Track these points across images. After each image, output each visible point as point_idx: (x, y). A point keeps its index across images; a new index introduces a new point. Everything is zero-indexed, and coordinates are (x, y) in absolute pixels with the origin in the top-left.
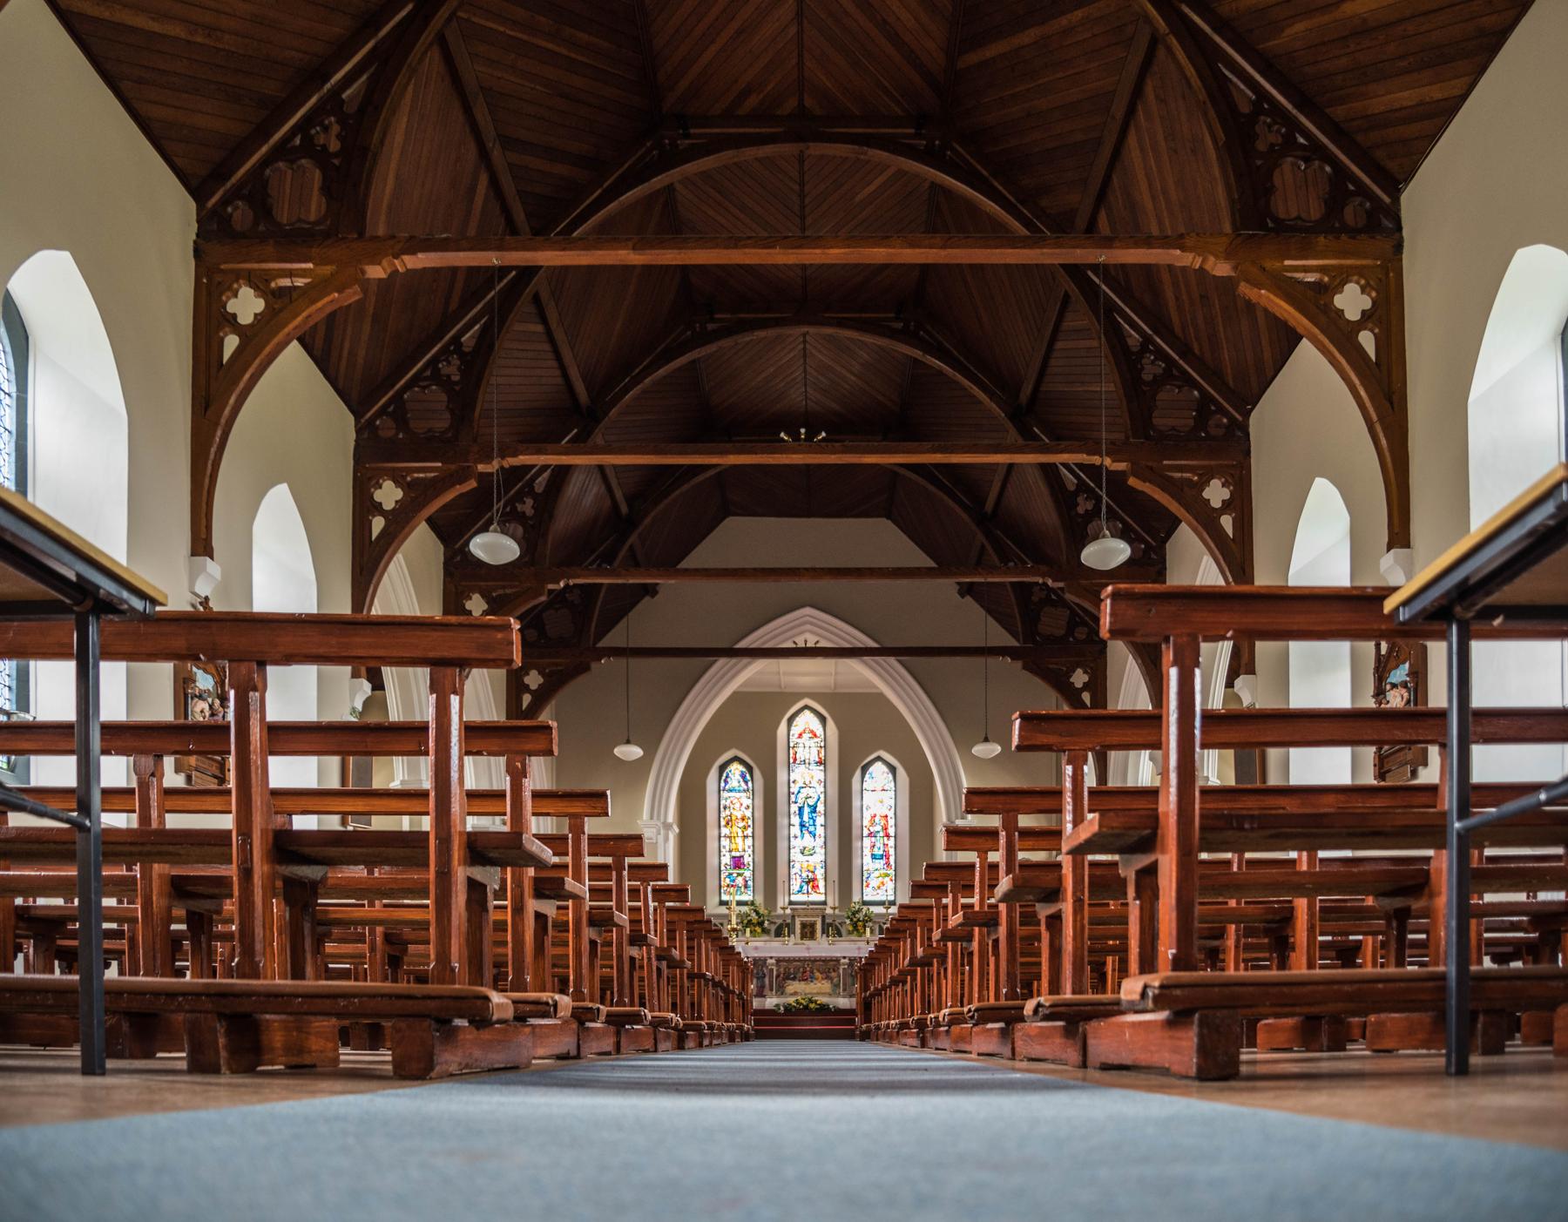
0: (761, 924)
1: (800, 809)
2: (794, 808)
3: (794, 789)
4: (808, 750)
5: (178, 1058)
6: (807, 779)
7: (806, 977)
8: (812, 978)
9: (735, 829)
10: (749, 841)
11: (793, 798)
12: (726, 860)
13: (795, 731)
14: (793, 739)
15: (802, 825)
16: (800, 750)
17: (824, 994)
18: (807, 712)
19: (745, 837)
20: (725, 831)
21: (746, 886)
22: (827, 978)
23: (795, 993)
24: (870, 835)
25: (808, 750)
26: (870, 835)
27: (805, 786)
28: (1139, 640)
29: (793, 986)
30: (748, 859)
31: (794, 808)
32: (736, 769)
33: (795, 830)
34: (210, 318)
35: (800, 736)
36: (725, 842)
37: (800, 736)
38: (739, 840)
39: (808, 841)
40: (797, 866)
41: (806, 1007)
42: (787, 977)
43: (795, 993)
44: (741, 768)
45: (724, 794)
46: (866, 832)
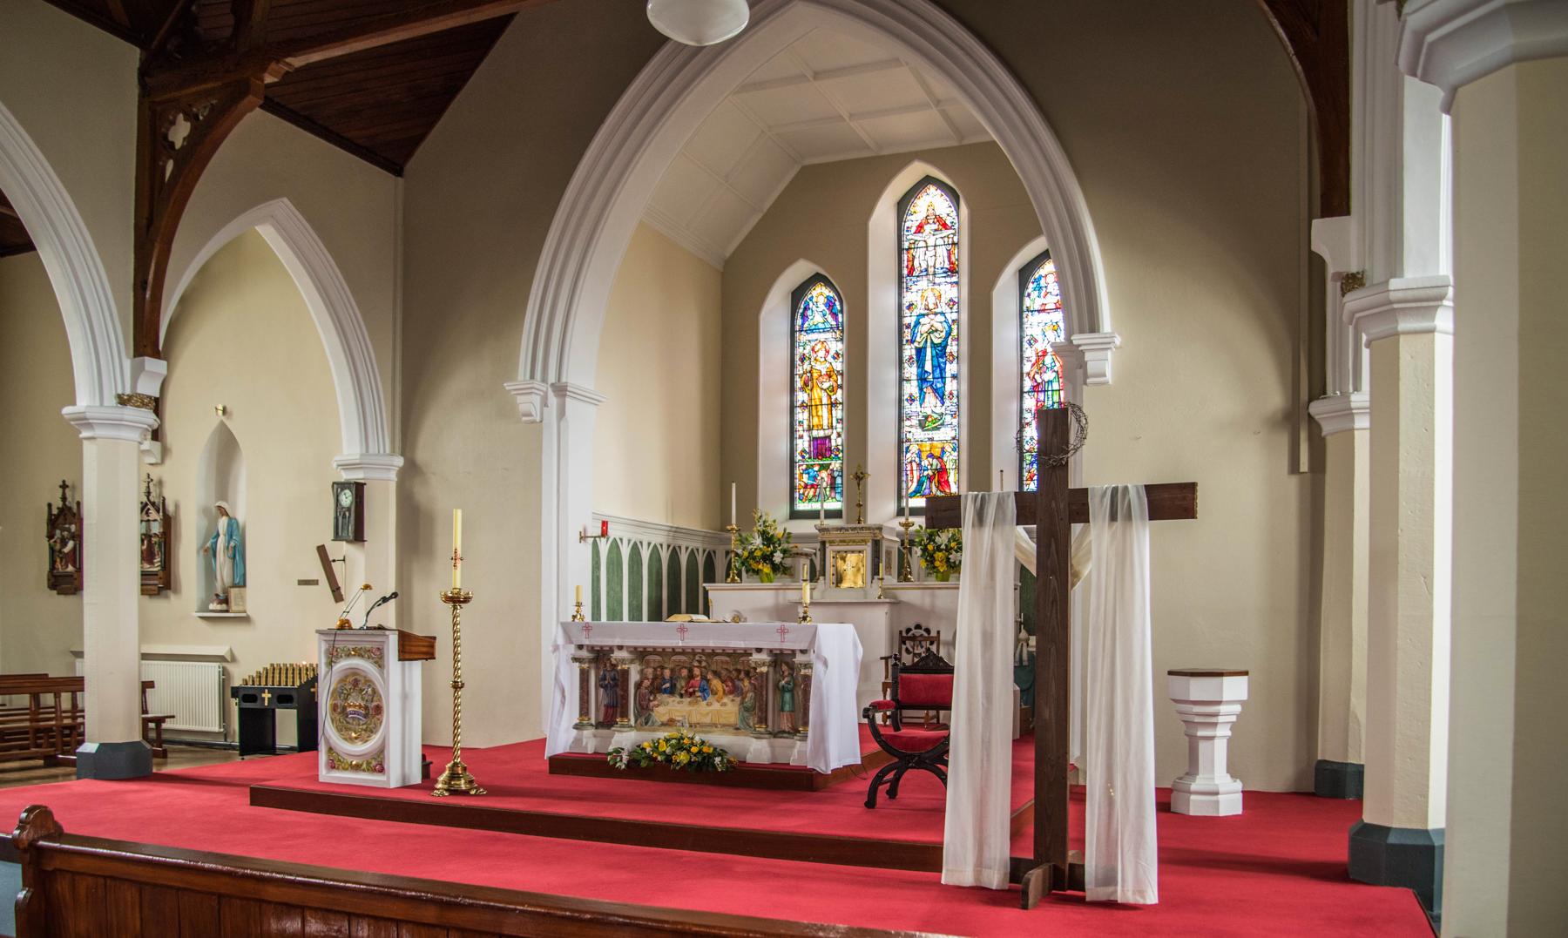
0: (767, 558)
1: (920, 352)
2: (909, 351)
3: (909, 320)
4: (931, 252)
5: (1076, 528)
6: (937, 299)
7: (695, 689)
8: (706, 690)
9: (817, 393)
10: (838, 413)
11: (907, 335)
12: (803, 444)
13: (912, 221)
14: (909, 236)
15: (922, 379)
16: (919, 253)
17: (725, 726)
18: (932, 190)
19: (833, 405)
20: (801, 397)
21: (833, 487)
22: (735, 690)
23: (670, 723)
24: (1036, 388)
25: (931, 252)
26: (1036, 388)
27: (929, 311)
28: (228, 423)
29: (669, 707)
30: (836, 442)
31: (909, 351)
32: (820, 294)
33: (911, 388)
34: (152, 143)
35: (920, 228)
36: (801, 415)
37: (920, 228)
38: (824, 412)
39: (931, 404)
40: (914, 448)
41: (669, 759)
42: (656, 689)
43: (670, 723)
44: (827, 292)
45: (802, 338)
46: (1028, 384)
